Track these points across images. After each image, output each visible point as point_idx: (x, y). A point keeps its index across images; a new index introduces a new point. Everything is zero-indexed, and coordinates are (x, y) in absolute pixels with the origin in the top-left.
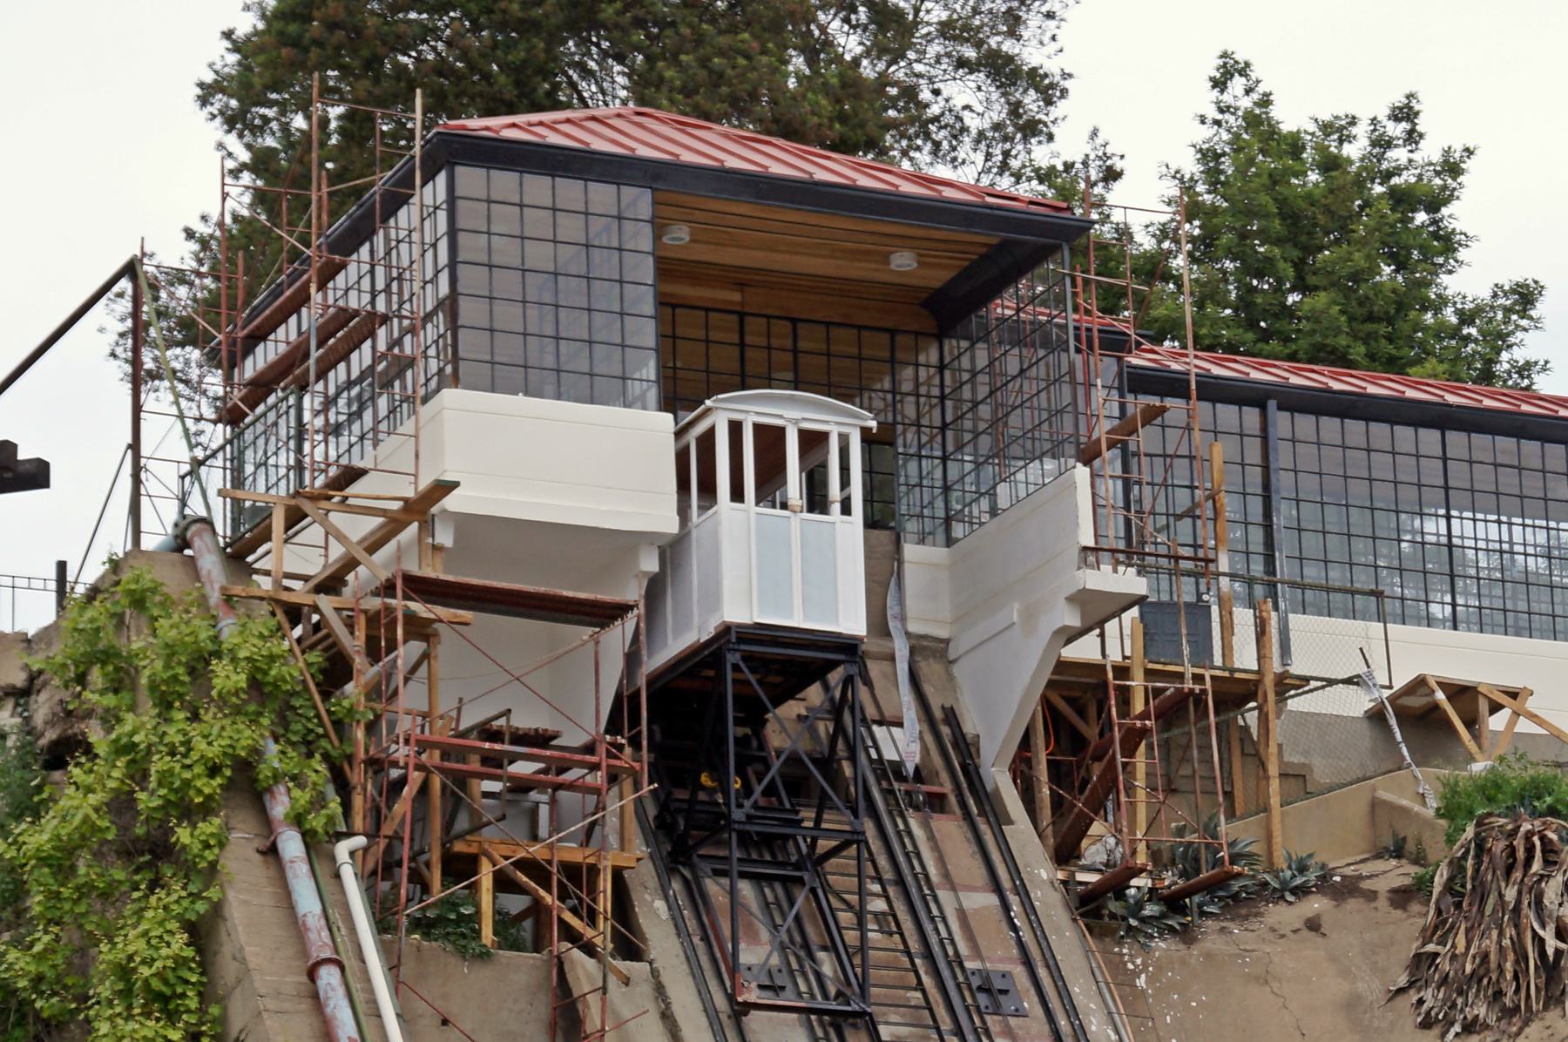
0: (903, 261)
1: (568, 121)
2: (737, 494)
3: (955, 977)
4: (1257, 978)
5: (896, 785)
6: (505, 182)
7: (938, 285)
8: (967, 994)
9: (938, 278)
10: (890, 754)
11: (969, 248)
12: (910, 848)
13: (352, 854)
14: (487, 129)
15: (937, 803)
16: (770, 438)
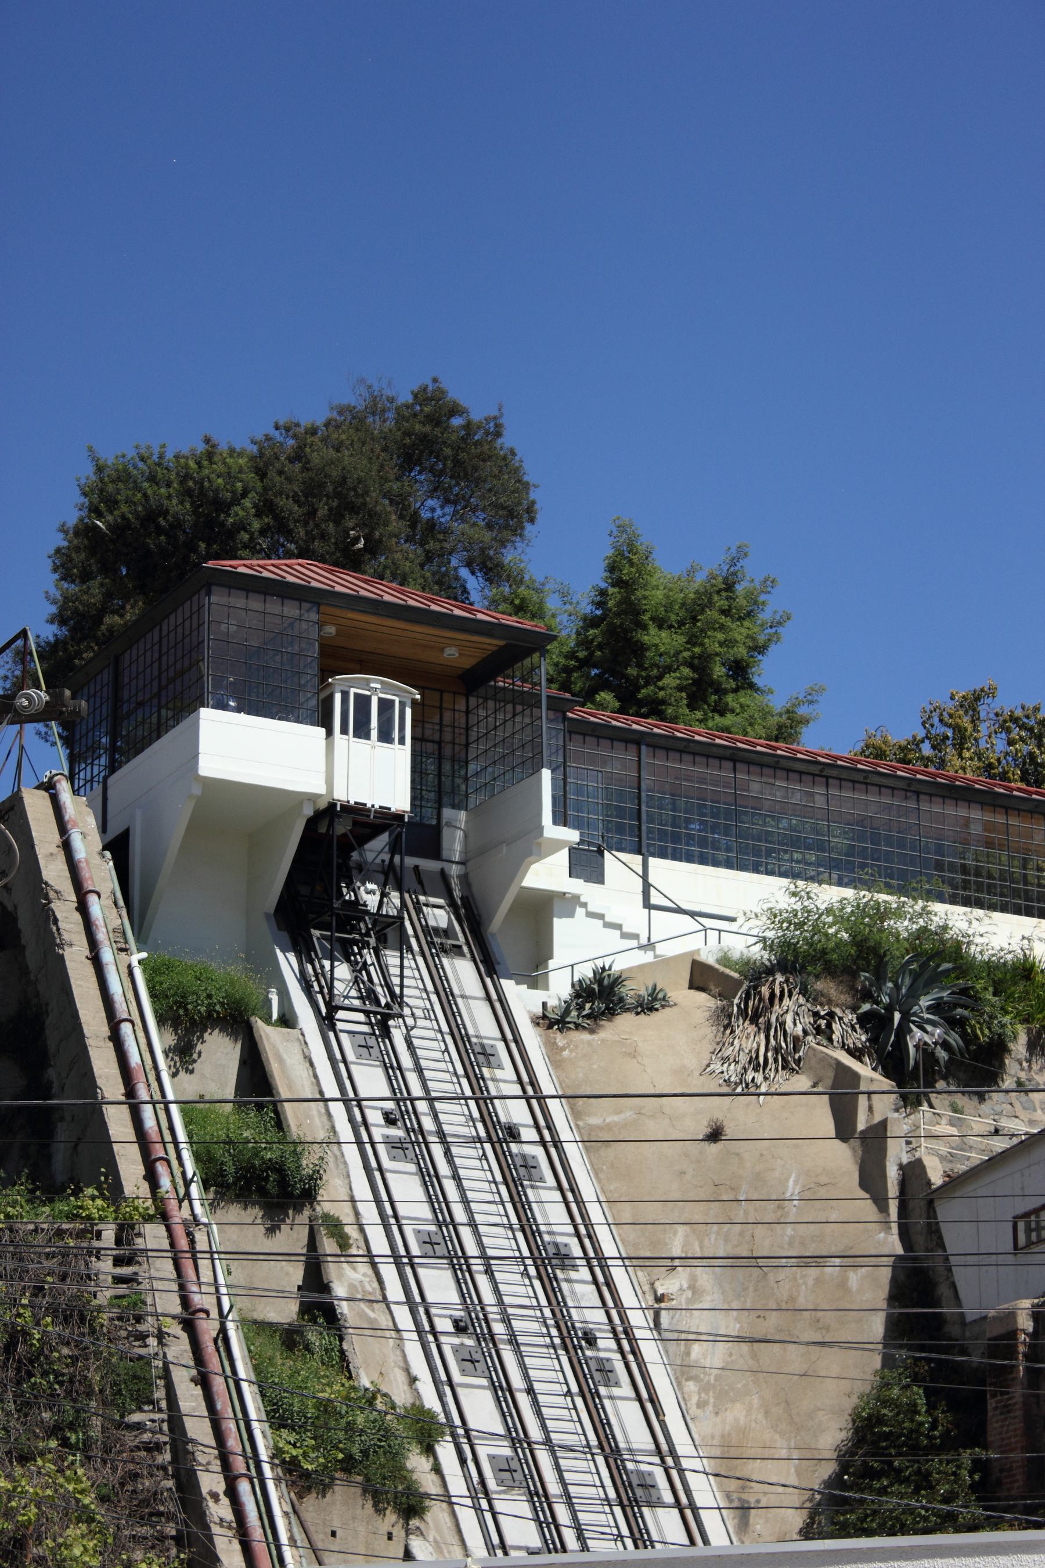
0: (451, 653)
1: (273, 565)
2: (344, 731)
3: (627, 1494)
4: (629, 1054)
5: (435, 940)
6: (238, 600)
7: (468, 667)
8: (472, 1055)
9: (468, 663)
10: (432, 923)
11: (486, 646)
12: (460, 1022)
13: (140, 962)
14: (231, 566)
15: (457, 951)
16: (363, 703)
